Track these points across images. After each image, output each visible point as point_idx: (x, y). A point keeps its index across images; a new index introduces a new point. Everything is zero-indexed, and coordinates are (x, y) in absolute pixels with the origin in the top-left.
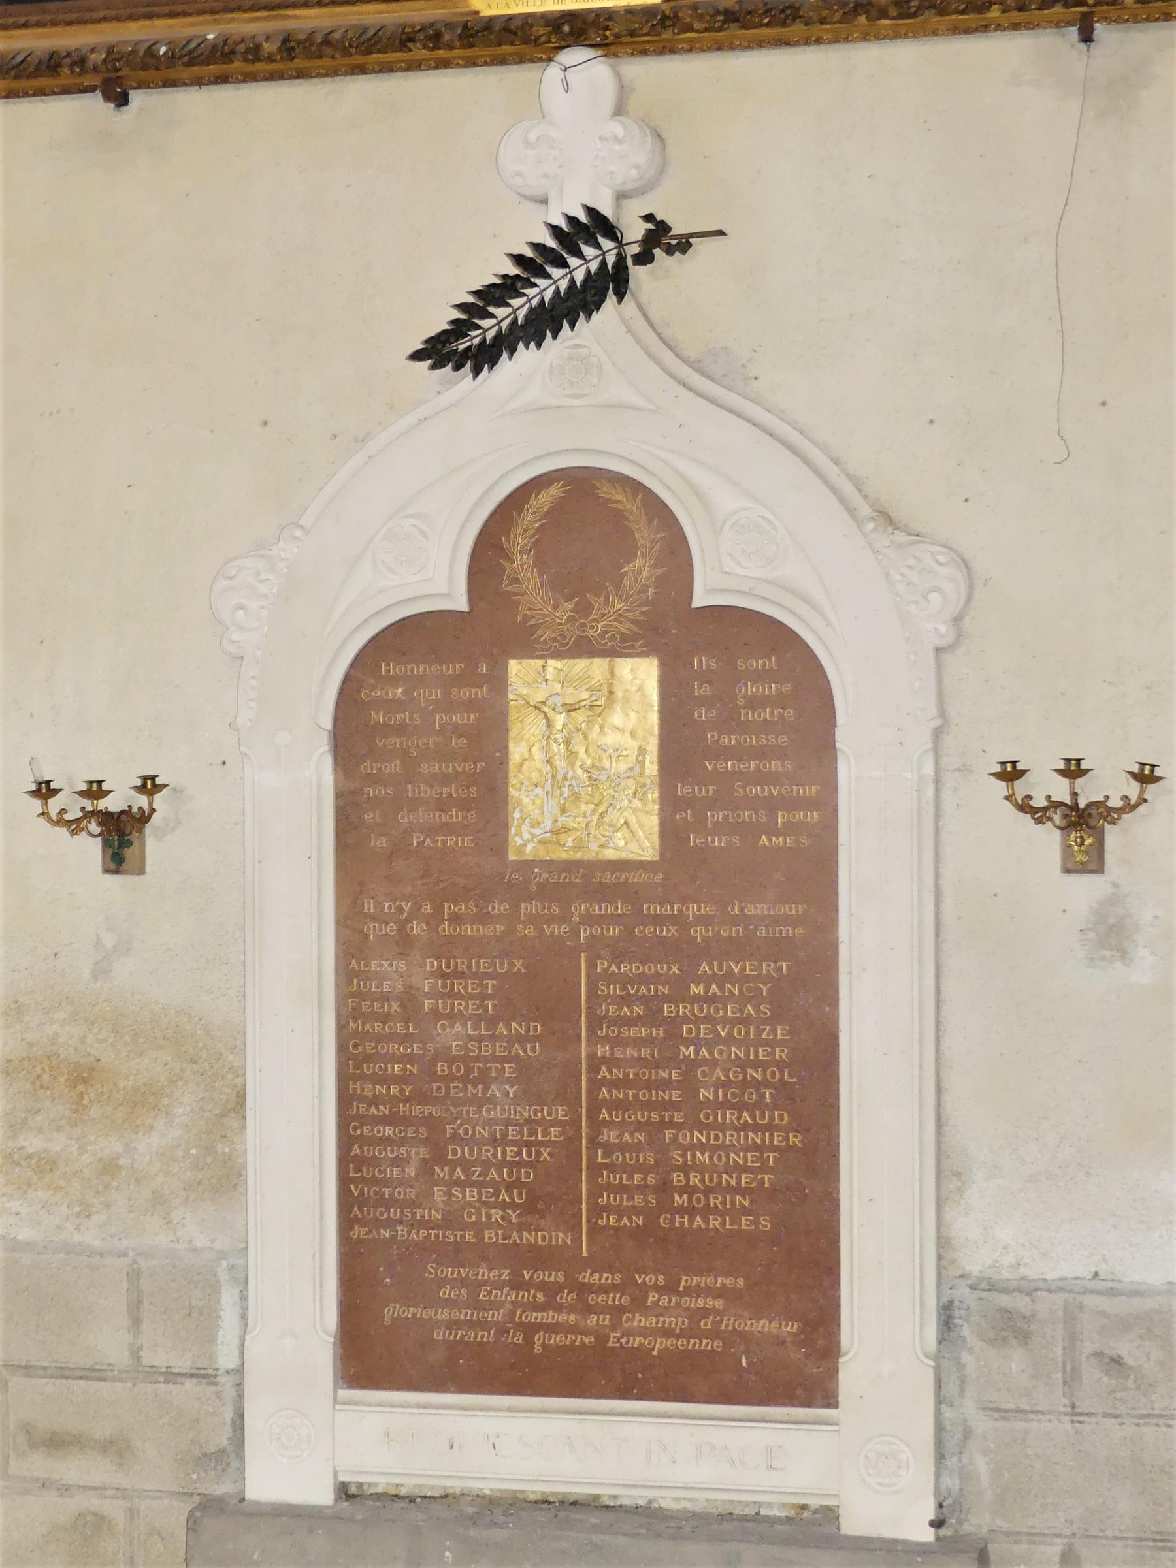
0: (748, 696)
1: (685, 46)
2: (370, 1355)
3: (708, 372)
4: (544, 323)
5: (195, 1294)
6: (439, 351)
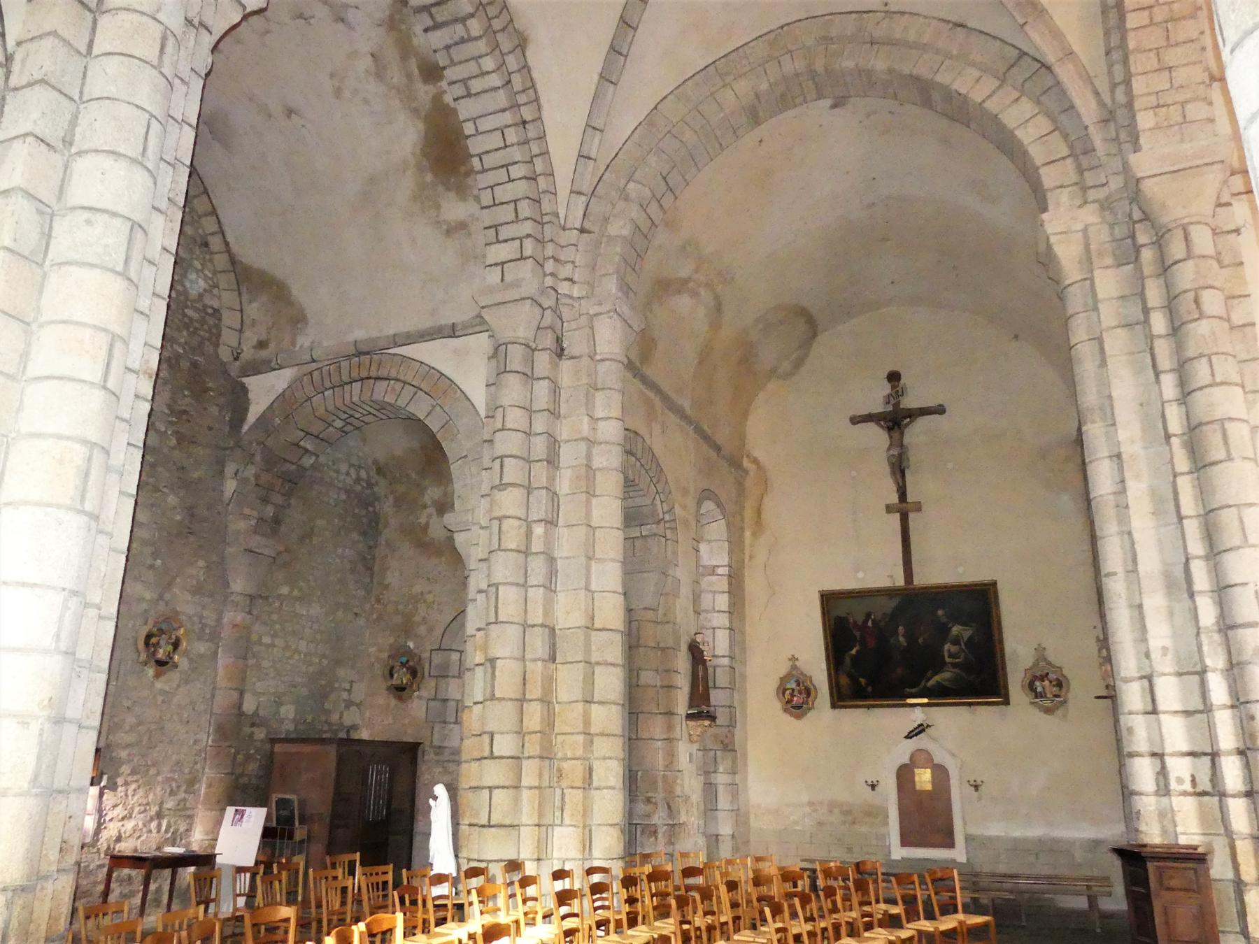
0: (940, 773)
1: (700, 667)
2: (904, 843)
3: (934, 739)
4: (916, 735)
5: (883, 837)
6: (906, 737)
